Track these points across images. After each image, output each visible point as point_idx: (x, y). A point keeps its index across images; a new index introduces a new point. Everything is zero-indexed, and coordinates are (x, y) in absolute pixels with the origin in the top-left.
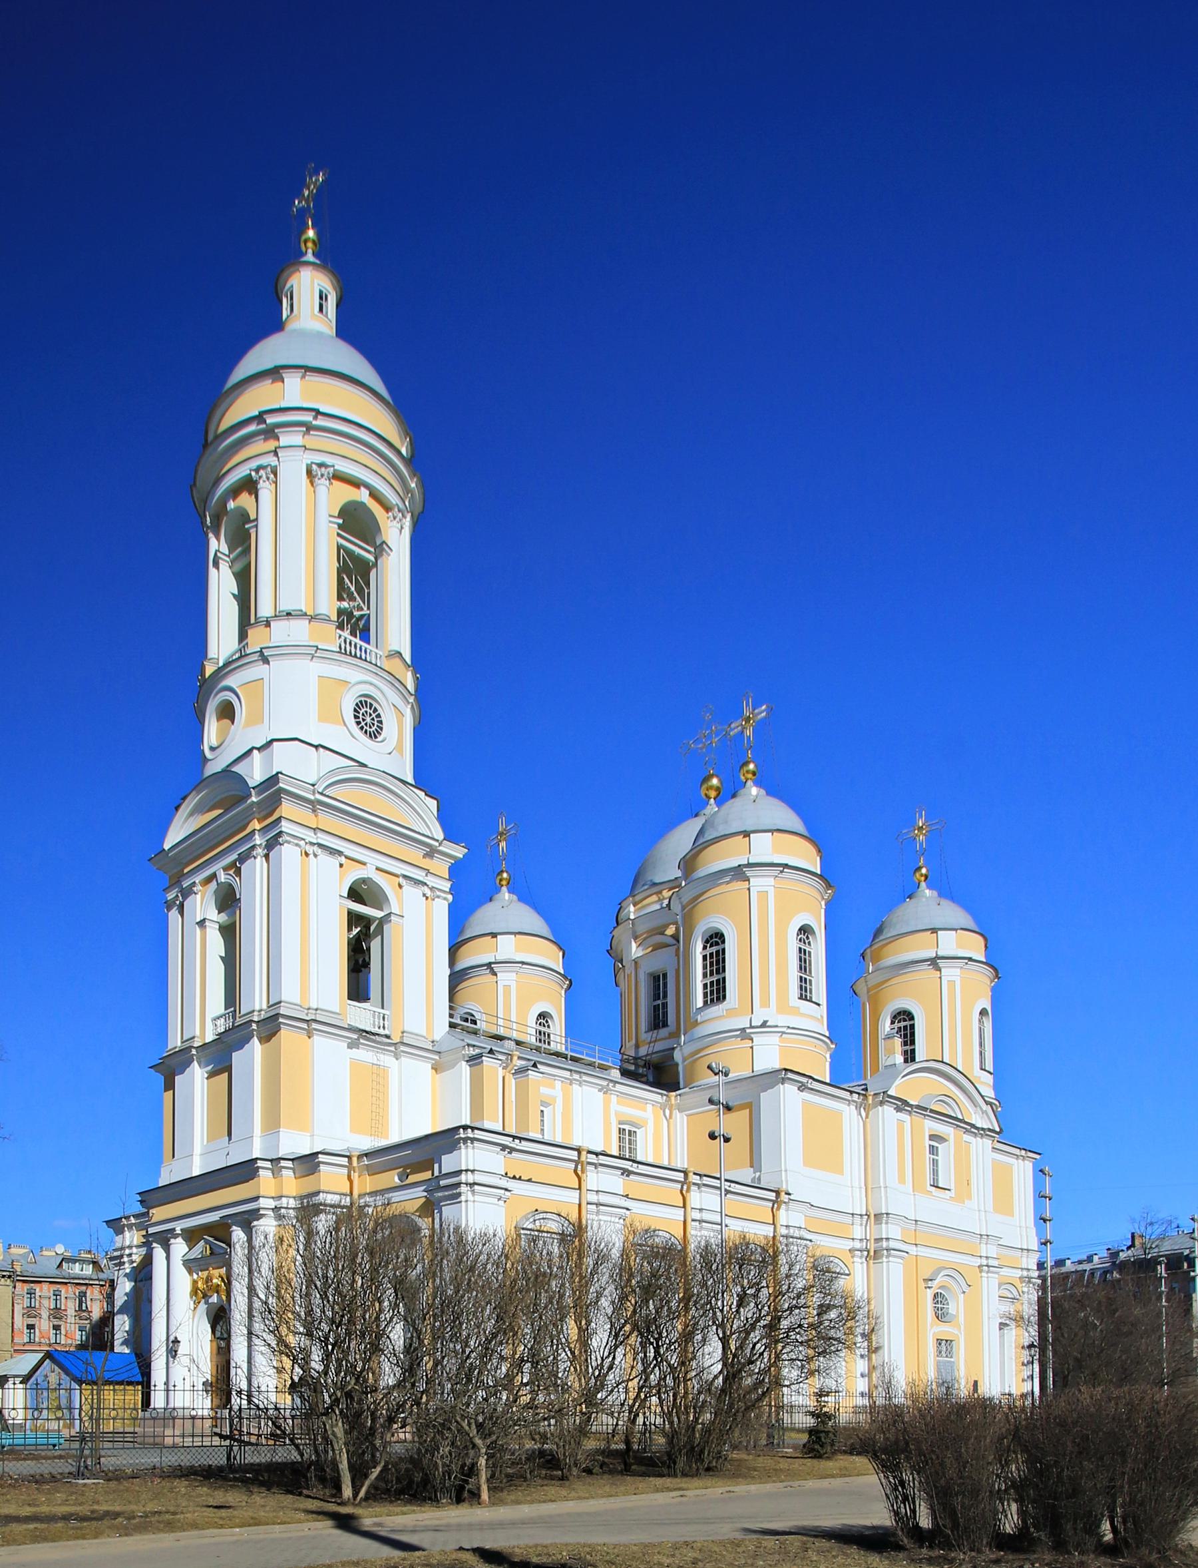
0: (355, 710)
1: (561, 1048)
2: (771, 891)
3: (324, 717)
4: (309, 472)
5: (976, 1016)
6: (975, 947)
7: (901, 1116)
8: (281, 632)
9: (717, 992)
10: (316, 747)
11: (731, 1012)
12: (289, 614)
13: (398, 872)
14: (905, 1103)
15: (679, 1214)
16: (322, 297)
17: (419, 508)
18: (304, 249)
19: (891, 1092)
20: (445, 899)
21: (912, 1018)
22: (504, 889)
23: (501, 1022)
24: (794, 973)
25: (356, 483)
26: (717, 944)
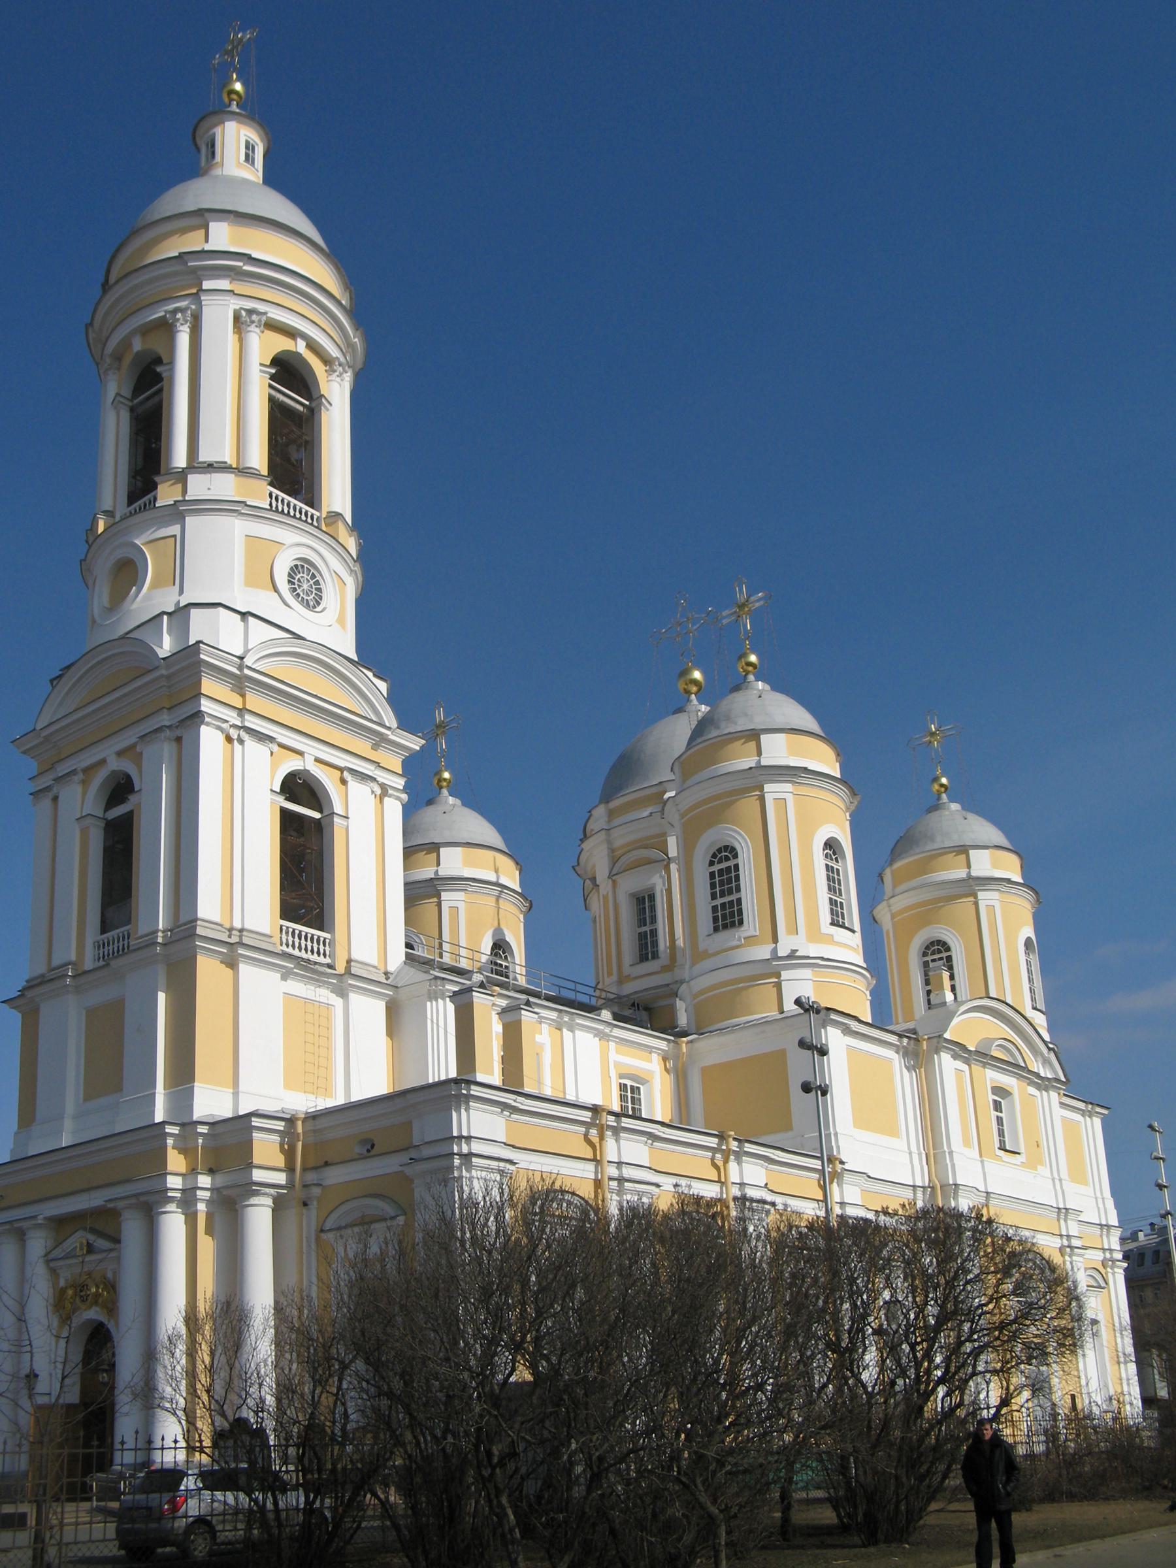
1: (522, 981)
2: (790, 798)
4: (237, 318)
8: (199, 486)
9: (728, 916)
10: (244, 615)
11: (751, 940)
13: (342, 764)
14: (963, 1047)
16: (249, 147)
17: (359, 365)
18: (226, 100)
19: (947, 1036)
20: (398, 798)
21: (948, 949)
22: (445, 792)
23: (463, 952)
24: (823, 896)
25: (291, 333)
26: (727, 859)
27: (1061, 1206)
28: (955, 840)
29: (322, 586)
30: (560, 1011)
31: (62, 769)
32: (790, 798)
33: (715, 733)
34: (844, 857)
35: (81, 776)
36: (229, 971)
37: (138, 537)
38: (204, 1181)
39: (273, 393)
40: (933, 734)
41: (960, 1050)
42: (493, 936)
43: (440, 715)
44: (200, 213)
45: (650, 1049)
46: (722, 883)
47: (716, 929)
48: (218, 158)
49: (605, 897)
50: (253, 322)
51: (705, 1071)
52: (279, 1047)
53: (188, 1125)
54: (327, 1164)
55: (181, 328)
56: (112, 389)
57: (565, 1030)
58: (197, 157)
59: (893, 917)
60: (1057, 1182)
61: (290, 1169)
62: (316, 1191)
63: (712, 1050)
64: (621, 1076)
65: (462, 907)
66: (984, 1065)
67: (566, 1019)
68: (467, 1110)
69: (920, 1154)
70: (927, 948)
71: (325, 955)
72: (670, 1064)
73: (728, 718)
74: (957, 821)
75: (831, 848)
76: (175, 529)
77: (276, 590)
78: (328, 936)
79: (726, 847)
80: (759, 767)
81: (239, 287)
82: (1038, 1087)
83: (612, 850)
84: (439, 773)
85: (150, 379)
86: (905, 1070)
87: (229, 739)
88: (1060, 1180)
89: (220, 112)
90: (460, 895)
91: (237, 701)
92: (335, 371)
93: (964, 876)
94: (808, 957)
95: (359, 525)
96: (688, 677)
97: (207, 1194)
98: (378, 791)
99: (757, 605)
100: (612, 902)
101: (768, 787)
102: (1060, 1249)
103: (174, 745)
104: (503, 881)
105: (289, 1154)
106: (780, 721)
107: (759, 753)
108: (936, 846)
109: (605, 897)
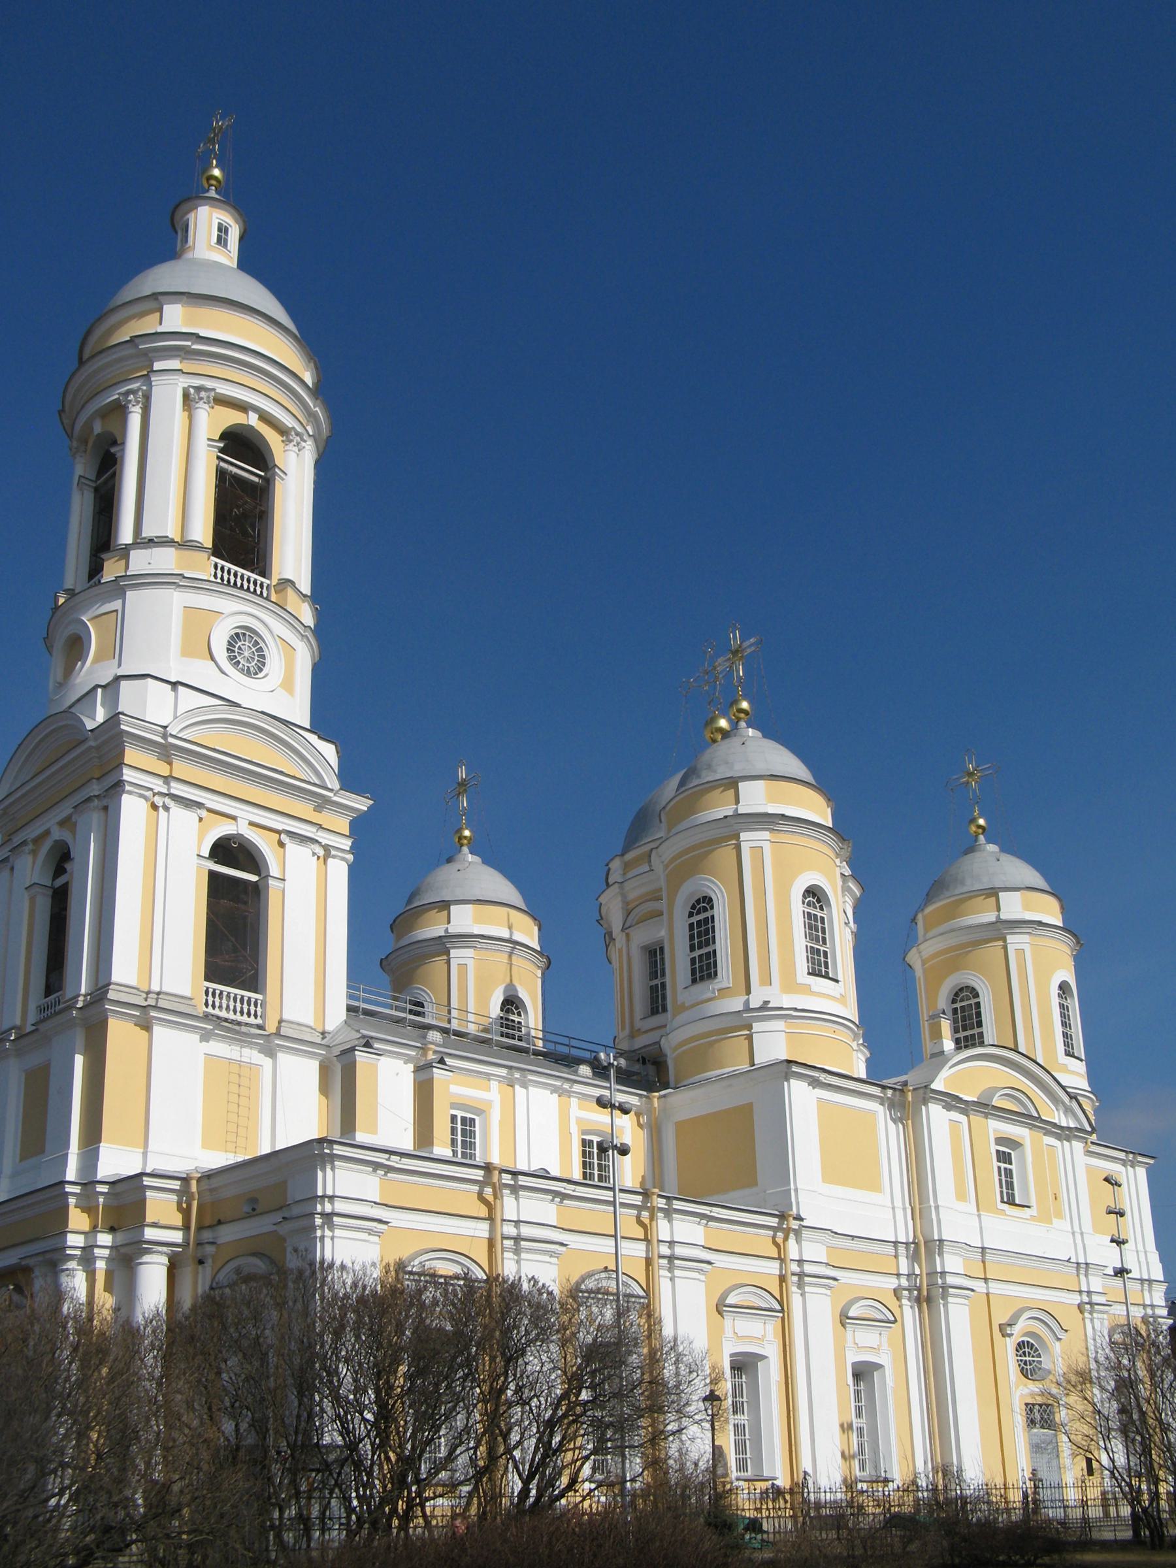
0: (230, 644)
2: (767, 846)
3: (187, 651)
4: (186, 396)
5: (1054, 991)
6: (1050, 912)
7: (955, 1115)
8: (140, 561)
9: (704, 969)
10: (175, 685)
12: (151, 541)
13: (280, 827)
16: (223, 229)
18: (206, 186)
19: (933, 1086)
20: (343, 859)
21: (977, 995)
22: (465, 849)
25: (243, 407)
26: (705, 910)
27: (1082, 1260)
28: (985, 883)
29: (266, 652)
30: (510, 1068)
31: (17, 840)
32: (767, 846)
33: (695, 782)
35: (31, 846)
36: (145, 1034)
37: (84, 614)
38: (105, 1239)
39: (222, 464)
40: (970, 774)
41: (952, 1101)
42: (505, 991)
43: (462, 773)
44: (155, 296)
46: (700, 935)
47: (694, 981)
48: (190, 242)
49: (620, 951)
50: (201, 399)
51: (679, 1125)
52: (174, 1109)
53: (88, 1183)
54: (220, 1222)
55: (133, 409)
56: (79, 470)
57: (517, 1087)
58: (170, 241)
59: (924, 963)
60: (1078, 1237)
61: (186, 1227)
62: (210, 1249)
63: (682, 1104)
64: (584, 1132)
65: (471, 964)
66: (986, 1116)
67: (517, 1075)
68: (333, 1169)
69: (904, 1209)
70: (956, 994)
71: (256, 1016)
73: (709, 766)
74: (994, 863)
75: (814, 895)
76: (116, 605)
77: (213, 658)
78: (259, 997)
79: (704, 898)
80: (737, 815)
81: (188, 366)
82: (1058, 1137)
83: (626, 903)
84: (460, 830)
85: (108, 463)
86: (890, 1123)
87: (154, 807)
88: (1082, 1234)
89: (193, 196)
90: (469, 952)
91: (164, 769)
92: (291, 441)
93: (993, 919)
94: (781, 1009)
95: (317, 596)
96: (715, 726)
97: (107, 1252)
98: (321, 852)
99: (749, 651)
100: (628, 952)
101: (744, 836)
102: (1079, 1306)
103: (102, 814)
104: (518, 937)
105: (186, 1213)
106: (760, 768)
107: (737, 802)
108: (965, 889)
109: (620, 951)
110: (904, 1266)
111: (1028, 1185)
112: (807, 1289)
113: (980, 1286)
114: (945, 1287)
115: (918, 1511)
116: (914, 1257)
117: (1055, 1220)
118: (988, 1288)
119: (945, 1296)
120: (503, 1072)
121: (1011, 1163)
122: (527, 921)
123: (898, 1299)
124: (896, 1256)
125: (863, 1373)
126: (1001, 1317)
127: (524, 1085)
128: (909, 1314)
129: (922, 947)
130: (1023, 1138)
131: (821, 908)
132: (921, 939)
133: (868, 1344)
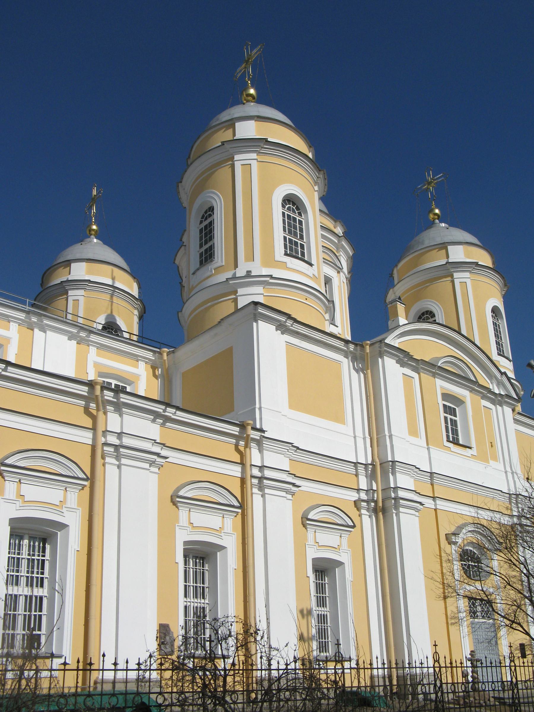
2: (469, 282)
5: (489, 314)
9: (207, 256)
15: (86, 437)
28: (439, 241)
34: (306, 212)
41: (404, 358)
45: (136, 358)
46: (206, 235)
51: (184, 375)
57: (36, 331)
66: (434, 375)
69: (364, 438)
72: (159, 372)
74: (442, 231)
82: (493, 402)
104: (118, 285)
110: (363, 483)
111: (469, 430)
112: (267, 491)
113: (429, 503)
114: (396, 499)
115: (372, 686)
116: (372, 477)
117: (491, 461)
118: (436, 505)
119: (397, 507)
120: (22, 316)
121: (456, 416)
122: (128, 278)
123: (358, 509)
124: (357, 475)
125: (324, 569)
126: (447, 528)
127: (43, 329)
128: (367, 522)
129: (396, 288)
130: (465, 397)
131: (300, 214)
132: (396, 281)
133: (327, 543)
